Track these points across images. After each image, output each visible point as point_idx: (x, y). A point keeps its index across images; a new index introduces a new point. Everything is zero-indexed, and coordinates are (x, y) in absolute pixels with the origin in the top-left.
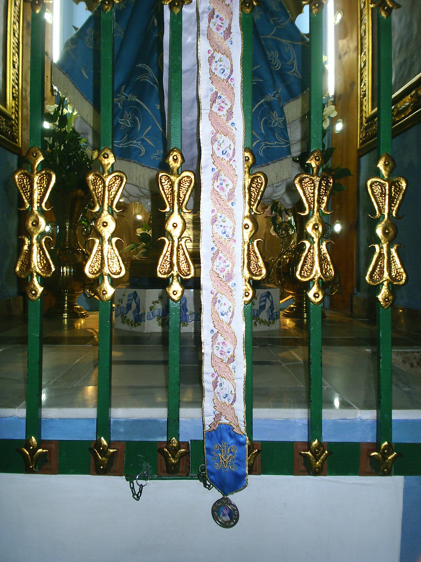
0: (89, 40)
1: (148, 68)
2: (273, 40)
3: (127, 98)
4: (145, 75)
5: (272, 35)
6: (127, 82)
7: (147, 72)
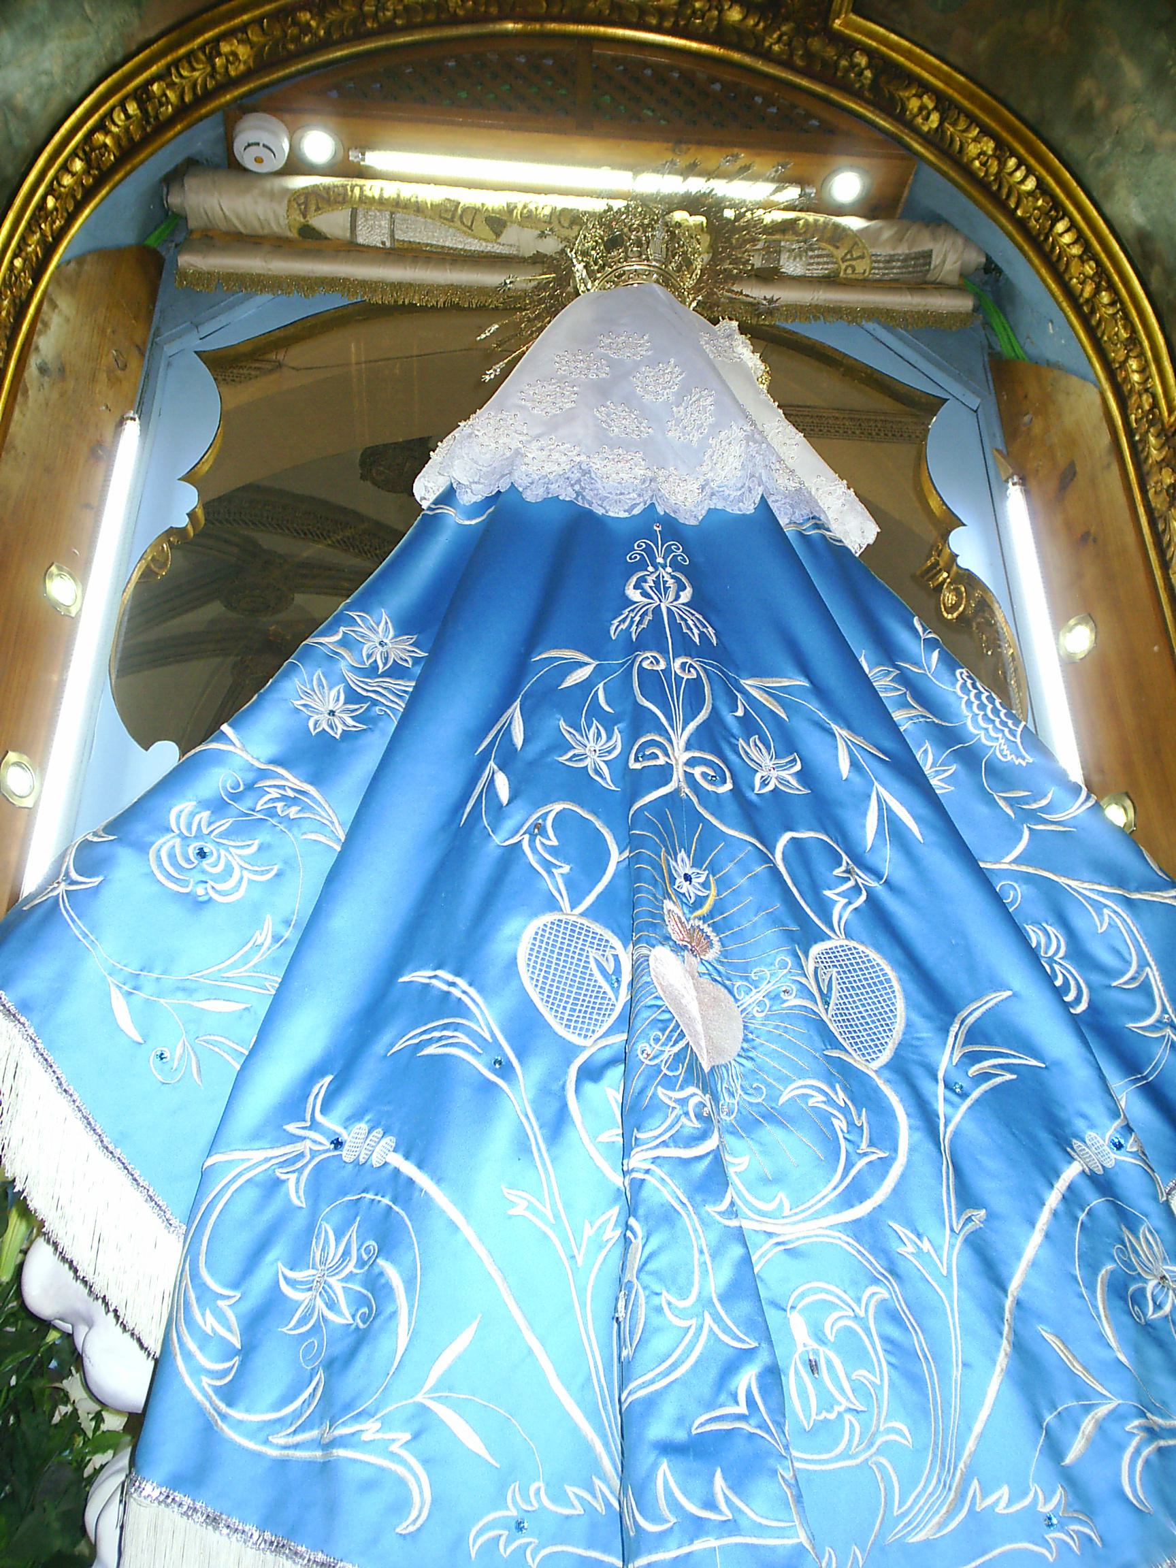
0: (172, 856)
1: (462, 988)
2: (1028, 879)
3: (338, 1144)
4: (445, 1027)
5: (1014, 862)
6: (340, 1064)
7: (460, 1009)
